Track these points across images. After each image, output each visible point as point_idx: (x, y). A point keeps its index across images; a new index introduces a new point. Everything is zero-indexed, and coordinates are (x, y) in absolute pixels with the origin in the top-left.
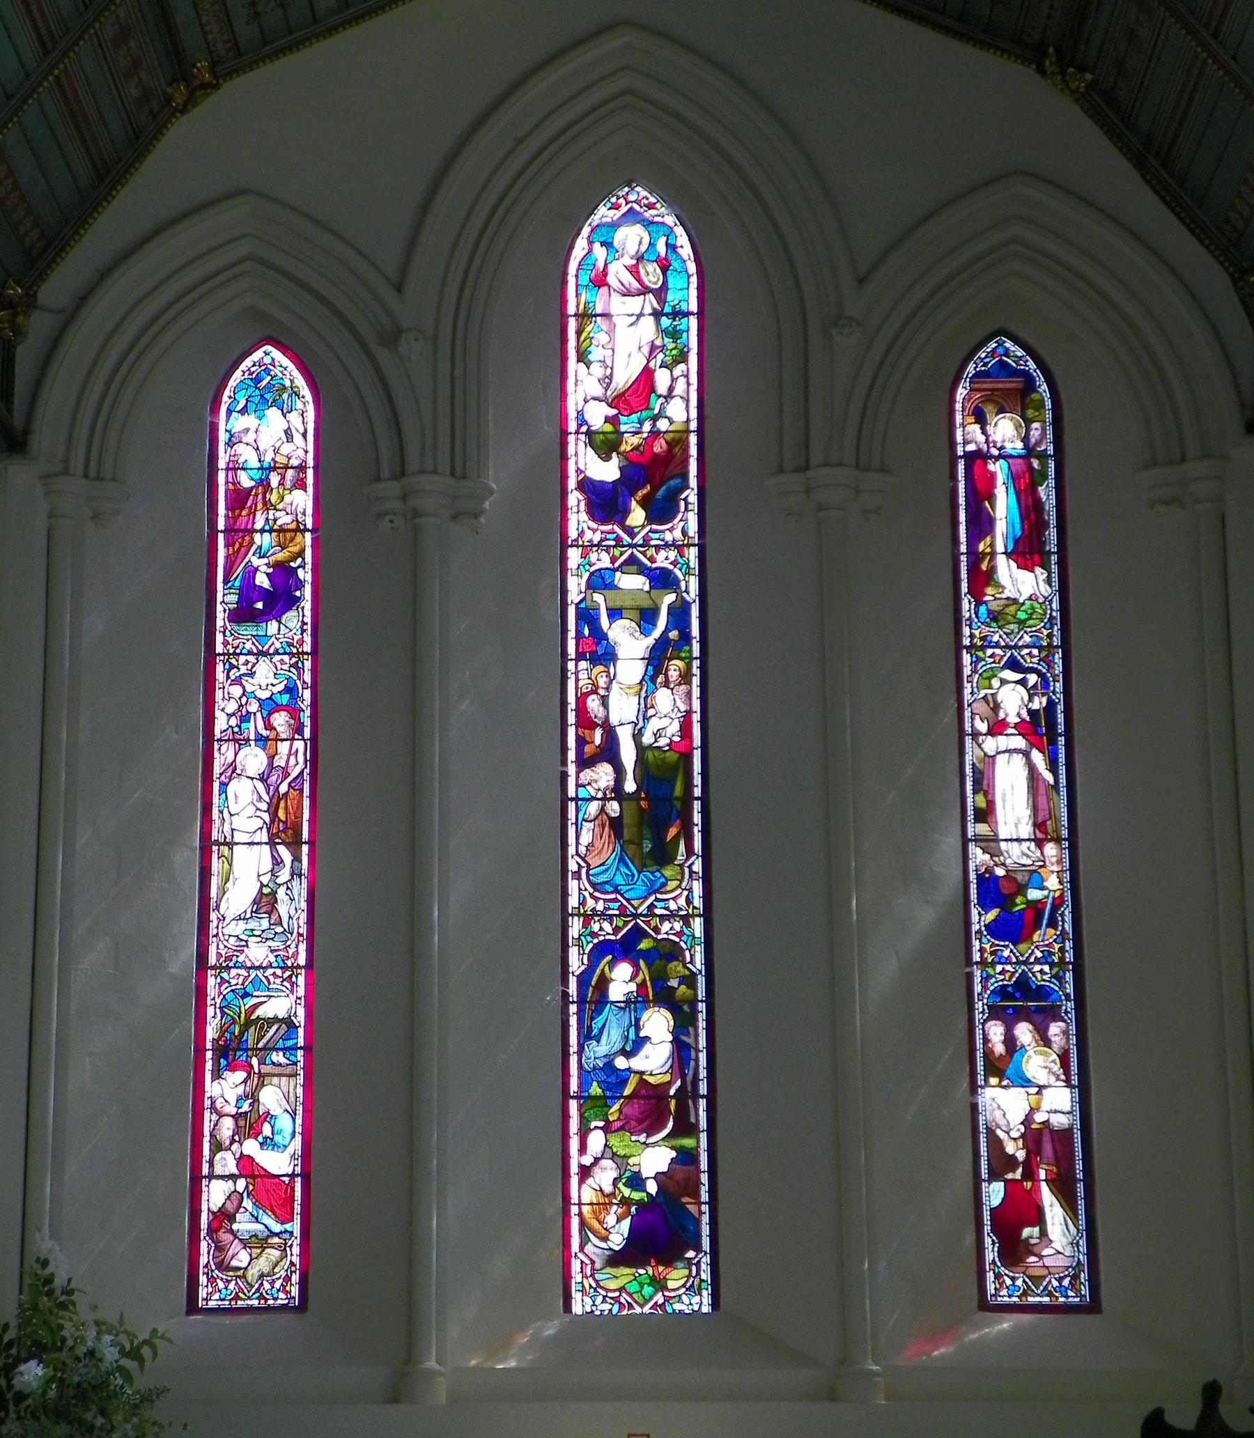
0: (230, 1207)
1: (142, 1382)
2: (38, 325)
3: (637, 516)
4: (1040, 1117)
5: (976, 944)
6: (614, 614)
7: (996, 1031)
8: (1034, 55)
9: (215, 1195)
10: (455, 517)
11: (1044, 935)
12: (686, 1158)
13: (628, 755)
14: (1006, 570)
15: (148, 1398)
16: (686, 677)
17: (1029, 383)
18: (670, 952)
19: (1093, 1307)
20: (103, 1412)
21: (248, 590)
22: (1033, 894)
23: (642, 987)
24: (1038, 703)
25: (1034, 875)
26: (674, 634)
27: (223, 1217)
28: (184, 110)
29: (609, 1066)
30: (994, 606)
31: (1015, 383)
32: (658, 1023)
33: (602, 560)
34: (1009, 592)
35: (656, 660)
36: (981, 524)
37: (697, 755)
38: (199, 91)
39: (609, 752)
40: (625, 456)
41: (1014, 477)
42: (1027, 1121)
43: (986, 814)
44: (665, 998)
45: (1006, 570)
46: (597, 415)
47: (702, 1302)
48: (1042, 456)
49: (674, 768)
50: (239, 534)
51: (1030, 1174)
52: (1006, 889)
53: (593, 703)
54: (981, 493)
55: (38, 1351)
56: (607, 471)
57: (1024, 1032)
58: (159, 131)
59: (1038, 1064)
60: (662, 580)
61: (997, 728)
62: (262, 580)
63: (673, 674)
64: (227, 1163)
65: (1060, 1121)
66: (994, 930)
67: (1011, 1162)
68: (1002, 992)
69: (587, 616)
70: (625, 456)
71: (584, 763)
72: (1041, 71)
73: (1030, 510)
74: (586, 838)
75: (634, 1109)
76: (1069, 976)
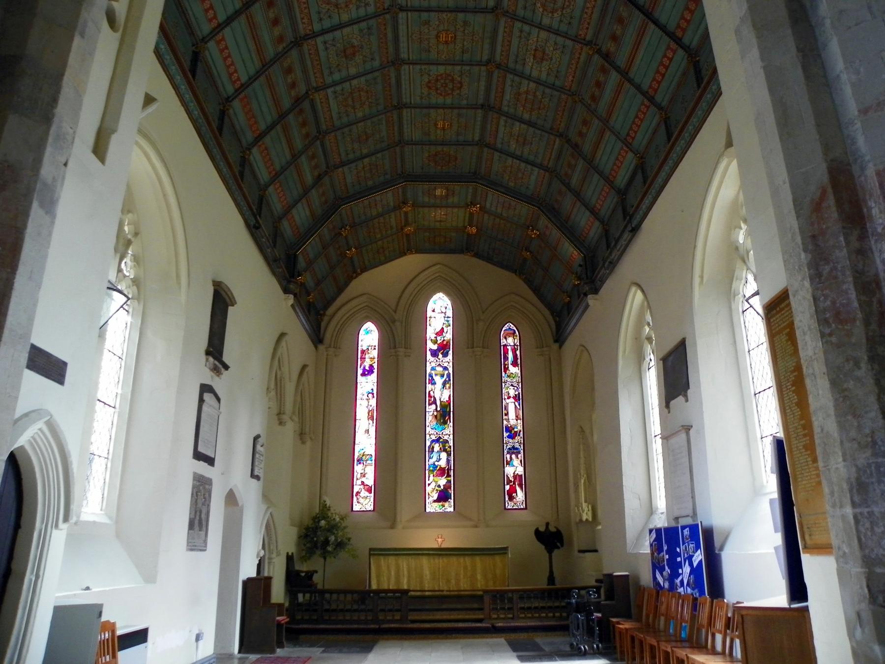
0: (360, 491)
1: (343, 525)
2: (326, 319)
3: (440, 356)
4: (516, 473)
5: (505, 439)
6: (436, 375)
7: (508, 456)
8: (515, 272)
9: (356, 489)
10: (405, 356)
11: (517, 438)
12: (449, 482)
13: (438, 403)
14: (511, 367)
15: (345, 528)
16: (450, 388)
17: (515, 332)
18: (447, 441)
19: (526, 508)
20: (337, 530)
21: (364, 369)
22: (516, 430)
23: (441, 448)
24: (517, 393)
25: (516, 426)
26: (447, 379)
27: (358, 493)
28: (355, 278)
29: (434, 464)
30: (508, 374)
31: (512, 332)
32: (444, 455)
33: (433, 364)
34: (511, 372)
35: (444, 384)
36: (506, 358)
37: (452, 413)
38: (358, 275)
39: (435, 402)
40: (438, 344)
41: (512, 350)
42: (514, 473)
43: (507, 414)
44: (445, 450)
45: (511, 367)
46: (433, 336)
47: (452, 509)
48: (517, 346)
49: (447, 406)
50: (363, 359)
51: (514, 483)
52: (510, 429)
53: (431, 393)
54: (506, 352)
55: (324, 518)
56: (435, 347)
57: (514, 456)
58: (350, 282)
59: (516, 462)
60: (445, 368)
61: (509, 398)
62: (367, 368)
63: (447, 387)
64: (359, 482)
65: (520, 473)
66: (509, 437)
67: (511, 481)
68: (509, 449)
69: (431, 375)
70: (438, 344)
71: (430, 404)
72: (516, 274)
73: (515, 356)
74: (430, 419)
75: (439, 472)
76: (522, 446)
